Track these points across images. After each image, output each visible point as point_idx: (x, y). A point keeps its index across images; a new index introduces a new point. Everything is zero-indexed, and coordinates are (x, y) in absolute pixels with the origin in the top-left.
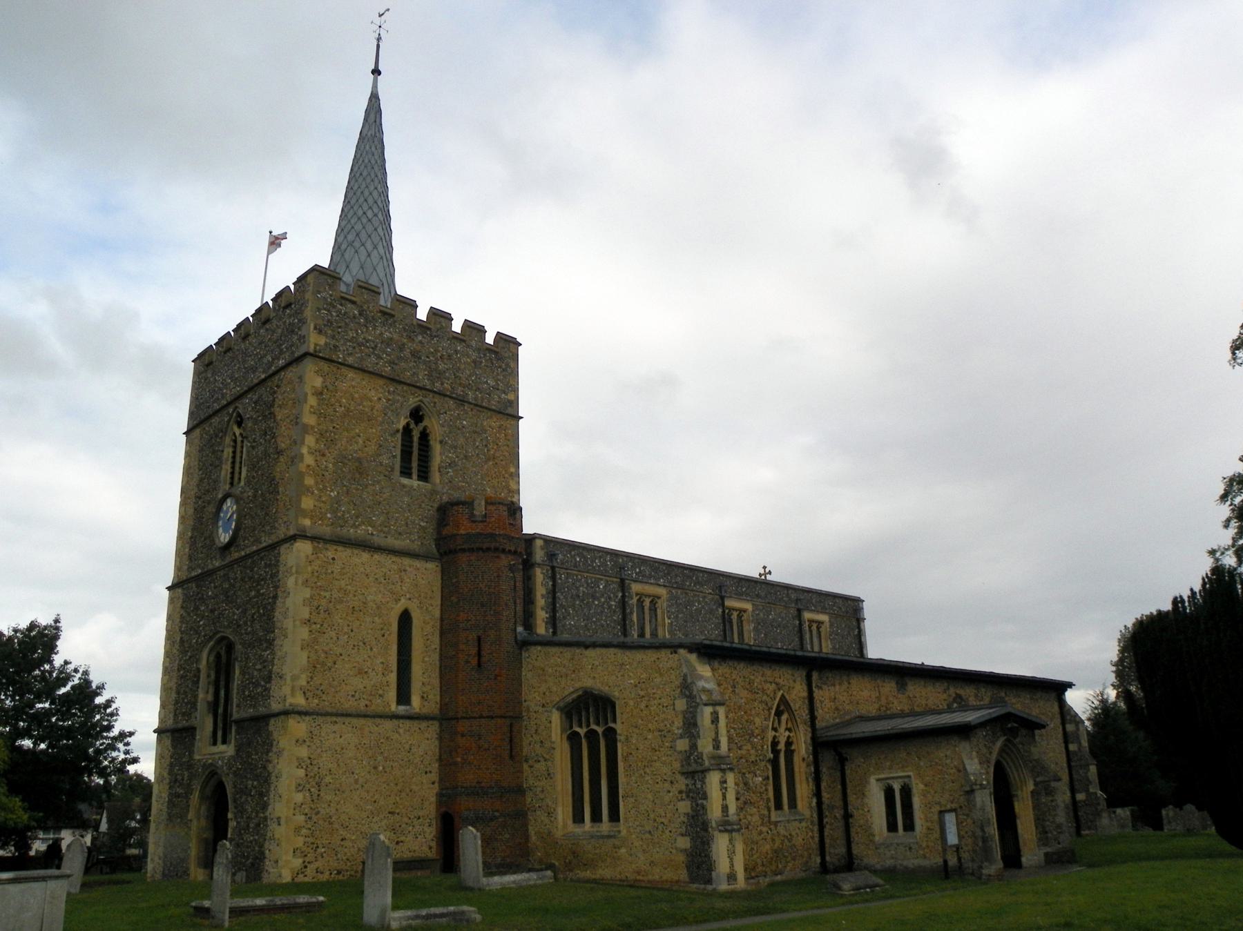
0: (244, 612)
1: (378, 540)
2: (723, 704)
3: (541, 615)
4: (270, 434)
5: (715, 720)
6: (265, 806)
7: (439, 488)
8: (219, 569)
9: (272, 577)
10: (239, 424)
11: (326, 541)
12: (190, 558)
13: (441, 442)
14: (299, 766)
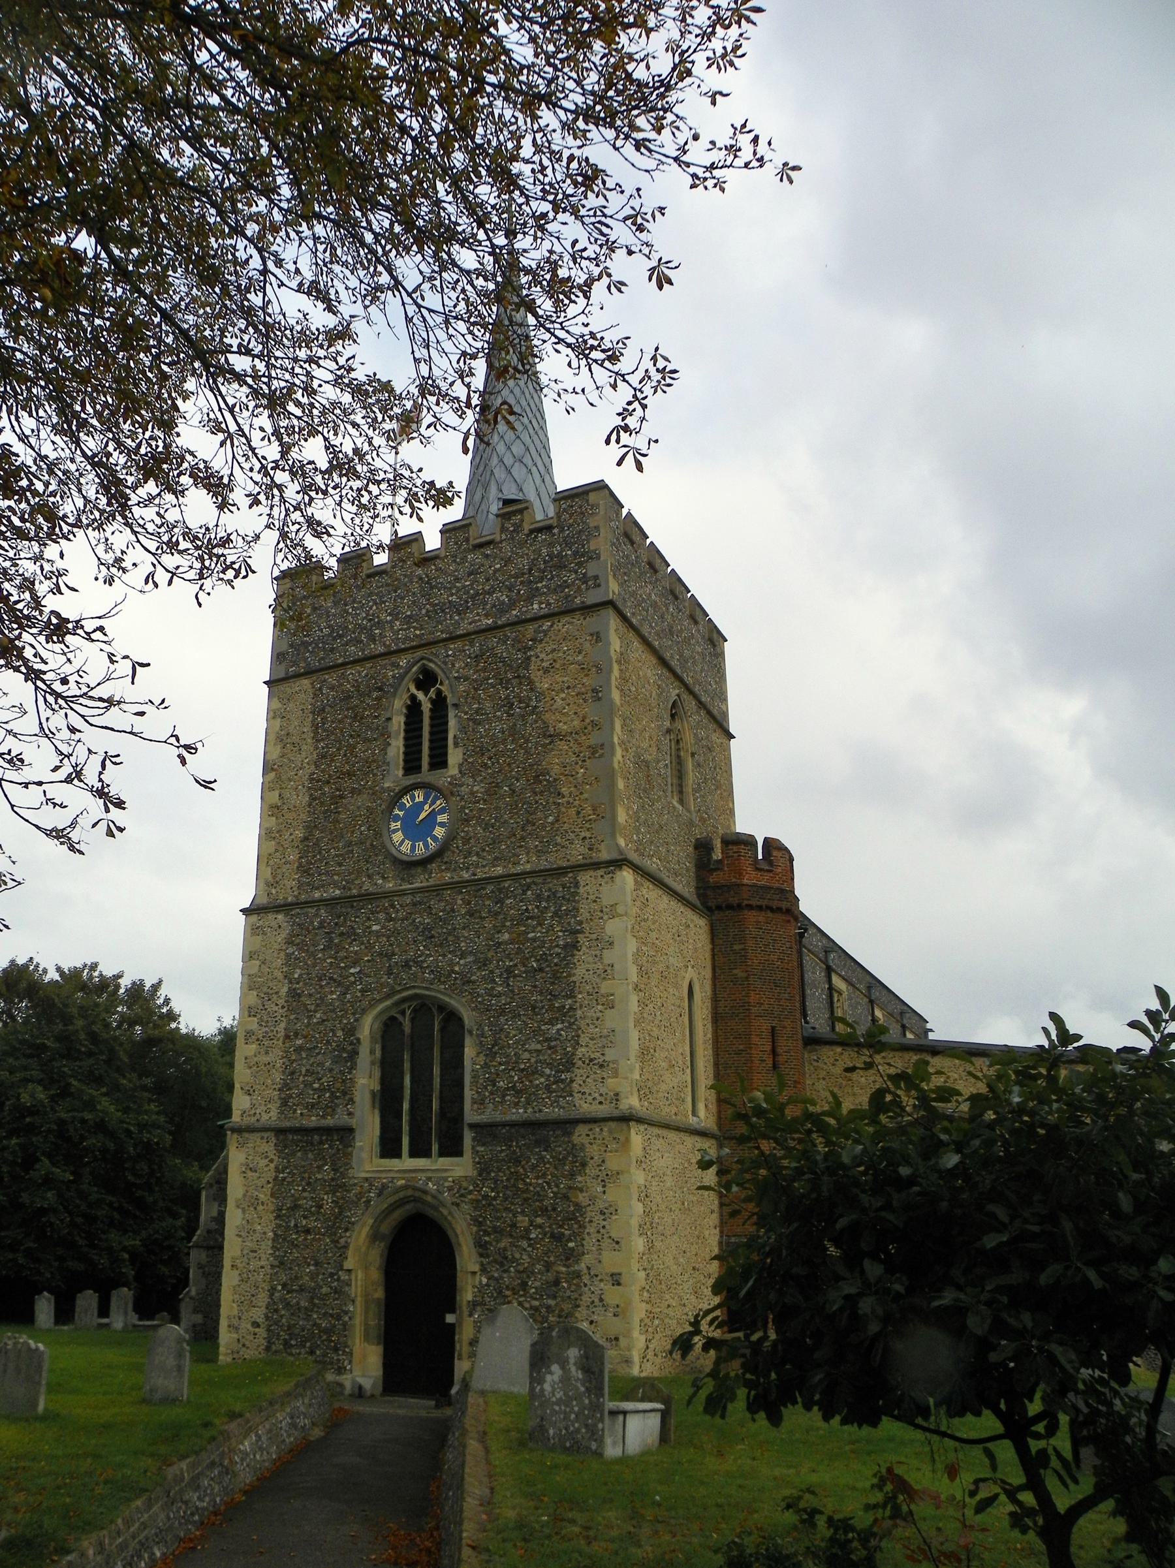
6: (571, 1256)
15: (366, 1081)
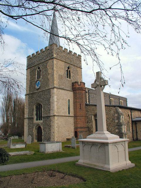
1: (65, 88)
3: (87, 100)
5: (123, 118)
6: (50, 130)
10: (39, 69)
15: (35, 113)
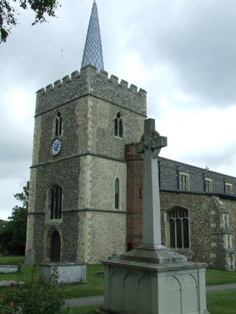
0: (65, 177)
2: (228, 213)
4: (73, 119)
5: (226, 218)
6: (77, 239)
7: (125, 139)
8: (53, 163)
9: (77, 166)
11: (96, 156)
12: (39, 158)
13: (126, 124)
14: (89, 227)
